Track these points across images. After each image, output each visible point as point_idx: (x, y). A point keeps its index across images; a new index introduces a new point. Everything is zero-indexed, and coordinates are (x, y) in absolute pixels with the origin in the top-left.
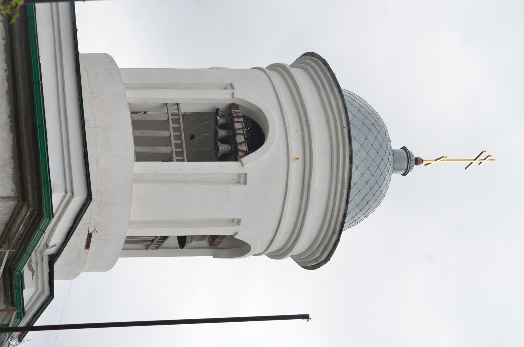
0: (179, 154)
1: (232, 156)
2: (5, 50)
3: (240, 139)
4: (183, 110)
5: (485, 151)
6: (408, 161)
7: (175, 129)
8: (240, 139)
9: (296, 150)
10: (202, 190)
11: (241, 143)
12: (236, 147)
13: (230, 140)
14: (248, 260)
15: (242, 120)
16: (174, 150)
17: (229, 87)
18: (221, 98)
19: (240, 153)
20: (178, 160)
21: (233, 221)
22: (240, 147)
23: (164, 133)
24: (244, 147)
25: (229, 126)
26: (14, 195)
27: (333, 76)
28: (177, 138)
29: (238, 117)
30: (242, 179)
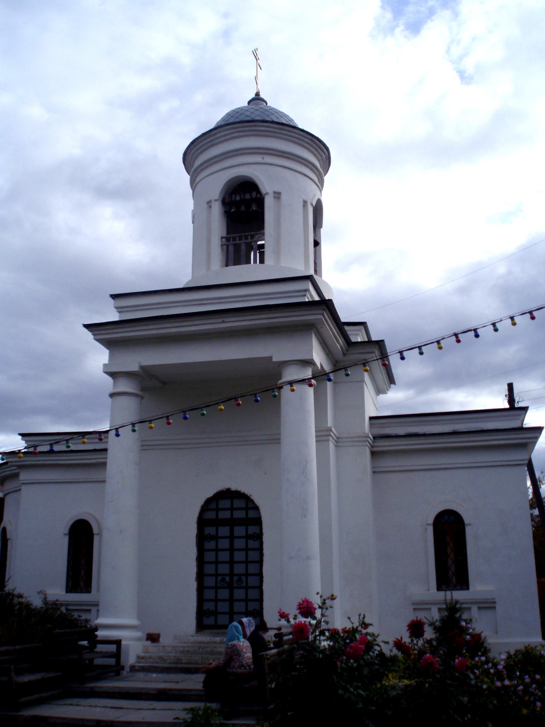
2: (197, 573)
3: (248, 196)
5: (256, 50)
7: (240, 239)
8: (248, 196)
9: (258, 159)
10: (281, 225)
11: (251, 196)
13: (252, 200)
16: (232, 242)
17: (209, 204)
18: (217, 209)
19: (258, 196)
21: (304, 206)
23: (243, 247)
24: (254, 194)
28: (234, 239)
29: (232, 198)
30: (277, 195)
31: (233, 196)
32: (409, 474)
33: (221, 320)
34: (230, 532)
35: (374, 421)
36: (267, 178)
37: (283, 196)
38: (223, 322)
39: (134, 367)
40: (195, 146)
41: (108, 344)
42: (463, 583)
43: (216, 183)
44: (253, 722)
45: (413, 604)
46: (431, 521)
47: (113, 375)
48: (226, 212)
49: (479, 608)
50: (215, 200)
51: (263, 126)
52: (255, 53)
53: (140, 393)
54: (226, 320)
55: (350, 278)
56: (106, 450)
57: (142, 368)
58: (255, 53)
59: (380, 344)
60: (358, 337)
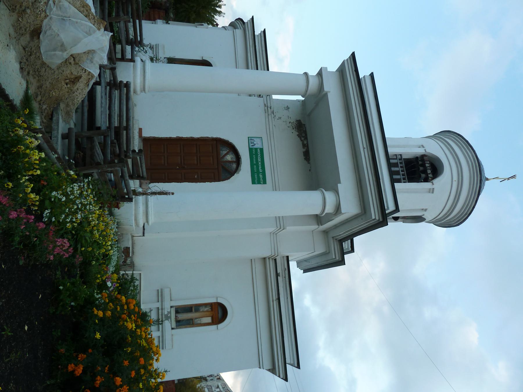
0: (404, 179)
1: (426, 180)
3: (429, 171)
4: (404, 157)
6: (487, 179)
8: (429, 171)
9: (455, 178)
12: (428, 175)
13: (425, 172)
14: (423, 223)
15: (428, 162)
18: (420, 151)
20: (404, 182)
21: (423, 209)
22: (429, 176)
24: (430, 176)
25: (423, 165)
26: (216, 17)
27: (467, 142)
28: (401, 163)
30: (431, 191)
31: (428, 162)
32: (251, 285)
33: (365, 146)
34: (203, 160)
35: (285, 259)
36: (443, 183)
37: (431, 195)
38: (364, 148)
39: (326, 88)
40: (456, 136)
41: (341, 70)
42: (180, 324)
43: (435, 149)
44: (275, 97)
45: (162, 290)
46: (220, 301)
47: (320, 74)
48: (417, 158)
49: (159, 337)
50: (425, 150)
51: (477, 180)
52: (514, 177)
53: (308, 93)
54: (366, 150)
55: (152, 327)
56: (257, 69)
57: (326, 95)
58: (514, 177)
59: (342, 262)
60: (346, 245)
